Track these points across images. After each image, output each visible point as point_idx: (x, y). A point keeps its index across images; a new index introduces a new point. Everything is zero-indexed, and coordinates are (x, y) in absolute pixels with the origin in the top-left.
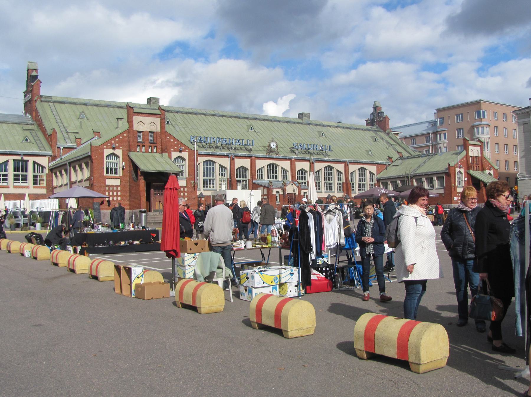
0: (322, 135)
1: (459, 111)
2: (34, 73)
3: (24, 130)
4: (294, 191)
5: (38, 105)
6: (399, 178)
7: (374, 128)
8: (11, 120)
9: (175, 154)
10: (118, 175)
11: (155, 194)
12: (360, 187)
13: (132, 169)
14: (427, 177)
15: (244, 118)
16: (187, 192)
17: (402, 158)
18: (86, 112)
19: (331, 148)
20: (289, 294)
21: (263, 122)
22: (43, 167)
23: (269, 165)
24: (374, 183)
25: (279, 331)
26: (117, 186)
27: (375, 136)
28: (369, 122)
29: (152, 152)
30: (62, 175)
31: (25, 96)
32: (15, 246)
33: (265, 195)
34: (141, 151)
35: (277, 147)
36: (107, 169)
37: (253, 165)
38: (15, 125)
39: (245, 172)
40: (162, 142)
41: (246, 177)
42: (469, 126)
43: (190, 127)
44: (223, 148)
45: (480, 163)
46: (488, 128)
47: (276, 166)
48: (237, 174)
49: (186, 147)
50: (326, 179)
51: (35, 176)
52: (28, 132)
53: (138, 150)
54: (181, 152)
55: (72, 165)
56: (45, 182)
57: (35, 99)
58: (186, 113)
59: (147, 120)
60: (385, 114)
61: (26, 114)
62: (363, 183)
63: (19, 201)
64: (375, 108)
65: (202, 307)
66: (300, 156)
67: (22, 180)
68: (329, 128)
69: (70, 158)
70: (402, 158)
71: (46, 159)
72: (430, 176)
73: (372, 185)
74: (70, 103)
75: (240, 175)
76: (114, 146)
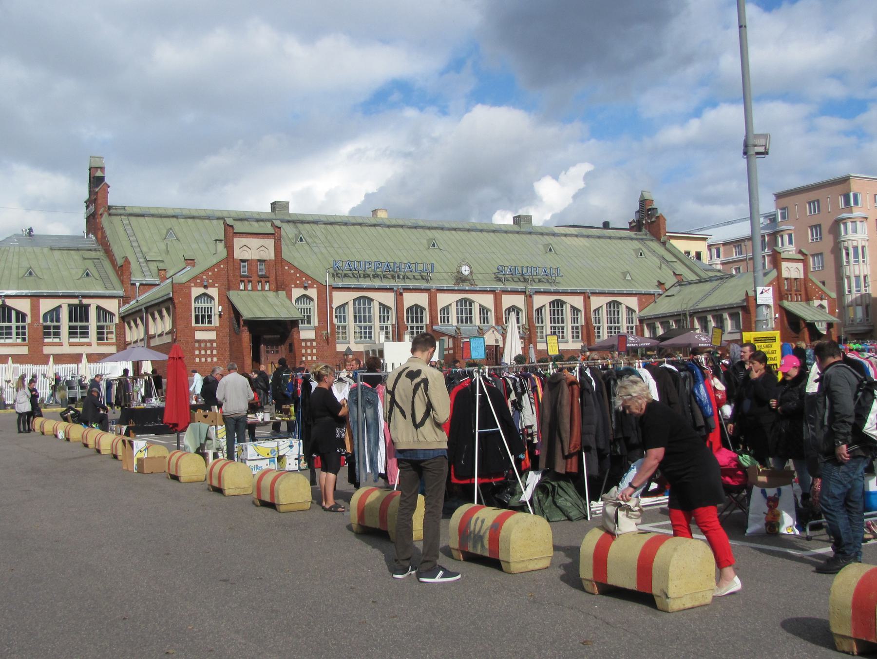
0: (550, 250)
1: (812, 196)
2: (99, 174)
3: (84, 258)
4: (497, 341)
5: (105, 221)
6: (672, 316)
7: (641, 235)
8: (66, 244)
9: (297, 292)
10: (213, 325)
11: (268, 352)
12: (611, 333)
13: (233, 315)
14: (715, 313)
15: (423, 228)
16: (317, 347)
17: (681, 282)
18: (176, 229)
20: (288, 468)
21: (454, 232)
22: (112, 314)
24: (634, 325)
25: (494, 563)
26: (211, 341)
27: (640, 249)
28: (634, 224)
29: (263, 289)
30: (162, 317)
31: (87, 207)
32: (49, 426)
33: (450, 349)
34: (246, 289)
35: (471, 273)
36: (197, 317)
37: (432, 302)
38: (72, 252)
39: (422, 313)
40: (278, 275)
41: (422, 321)
42: (830, 222)
43: (335, 245)
44: (384, 277)
45: (803, 289)
46: (865, 224)
47: (471, 302)
49: (314, 281)
50: (553, 320)
51: (99, 327)
52: (90, 261)
53: (242, 287)
54: (305, 288)
55: (150, 310)
56: (114, 336)
57: (100, 212)
58: (331, 224)
59: (254, 242)
60: (659, 212)
61: (88, 234)
62: (617, 325)
63: (75, 365)
64: (643, 202)
65: (511, 560)
66: (509, 286)
67: (81, 333)
68: (563, 238)
69: (157, 296)
70: (681, 282)
71: (116, 301)
72: (719, 313)
73: (632, 328)
74: (153, 216)
75: (412, 317)
76: (205, 284)
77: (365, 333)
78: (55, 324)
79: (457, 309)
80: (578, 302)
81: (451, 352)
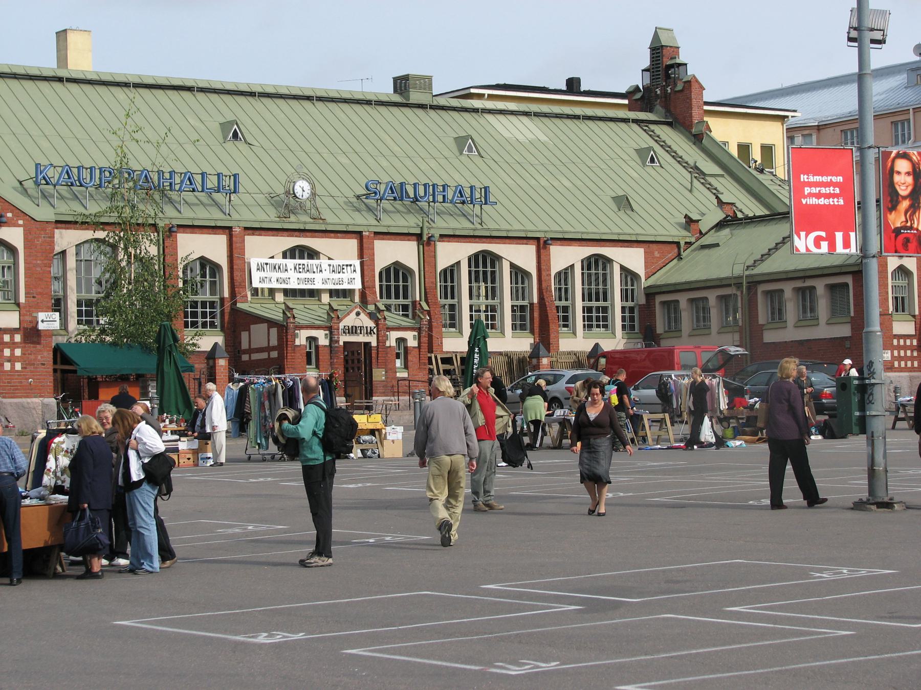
19: (242, 179)
23: (474, 259)
27: (650, 148)
35: (314, 194)
37: (234, 252)
48: (381, 286)
64: (657, 50)
70: (731, 221)
77: (598, 319)
79: (470, 272)
80: (524, 256)
81: (274, 354)
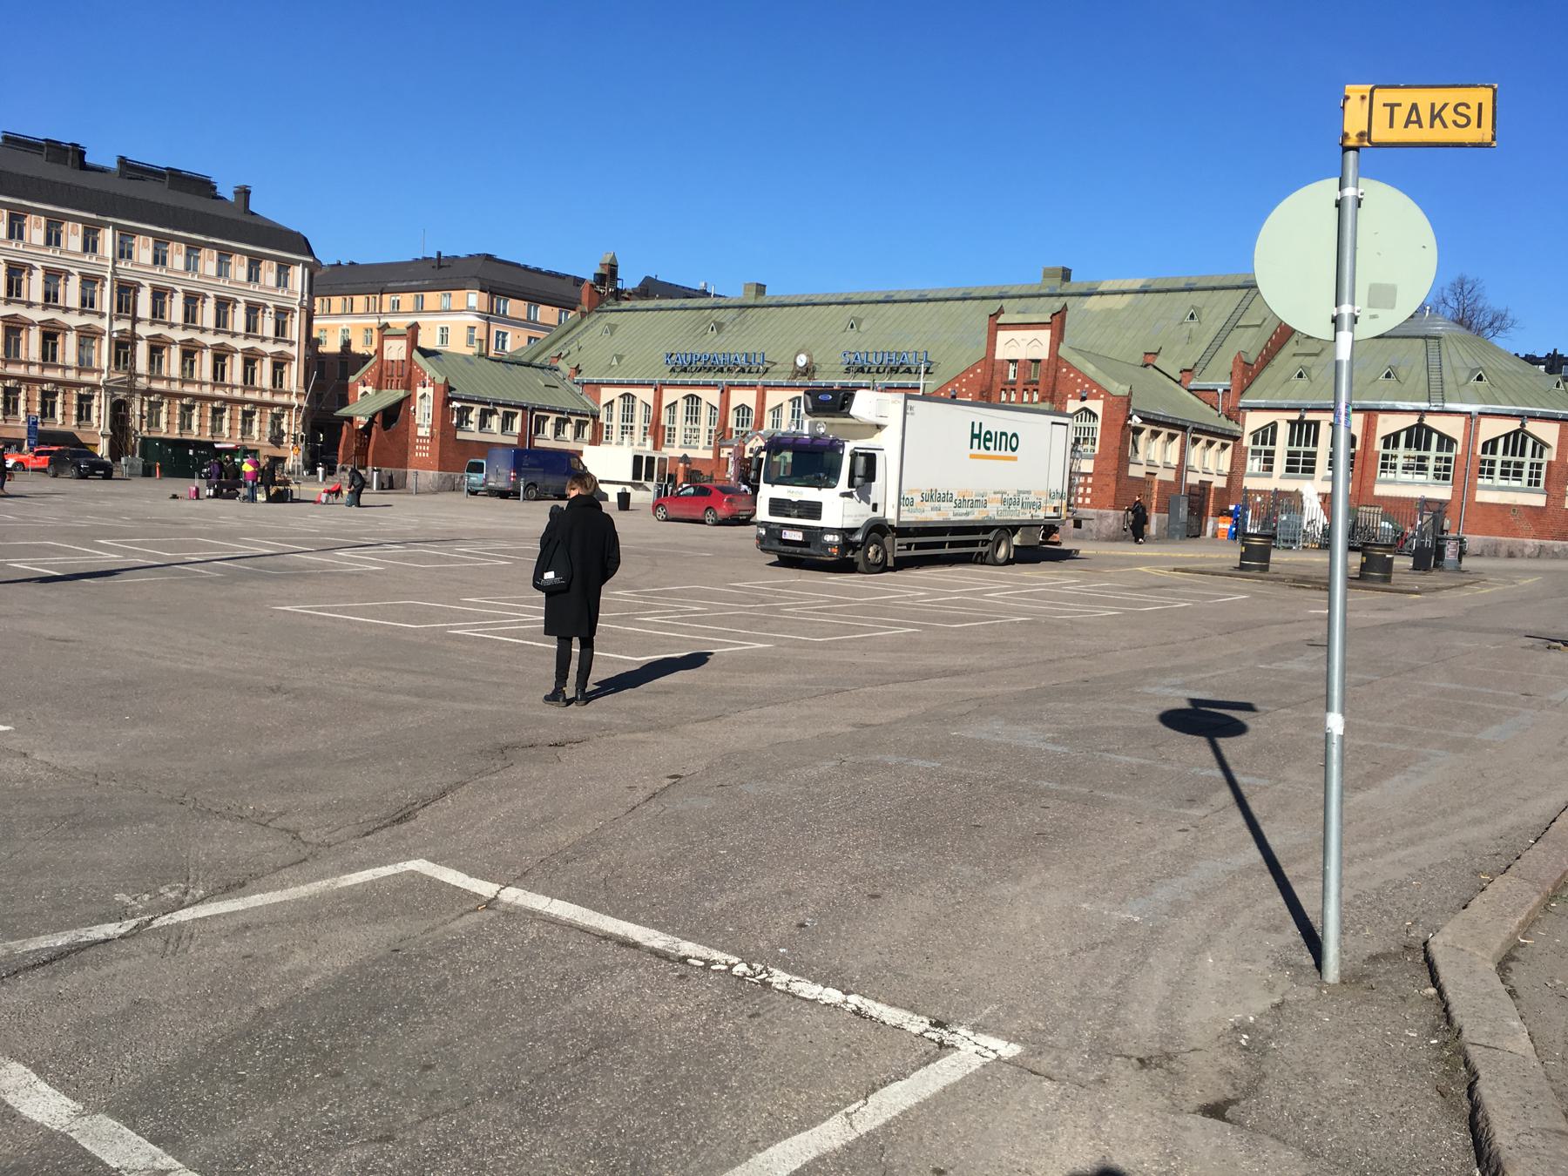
73: (1539, 466)
78: (1268, 447)
